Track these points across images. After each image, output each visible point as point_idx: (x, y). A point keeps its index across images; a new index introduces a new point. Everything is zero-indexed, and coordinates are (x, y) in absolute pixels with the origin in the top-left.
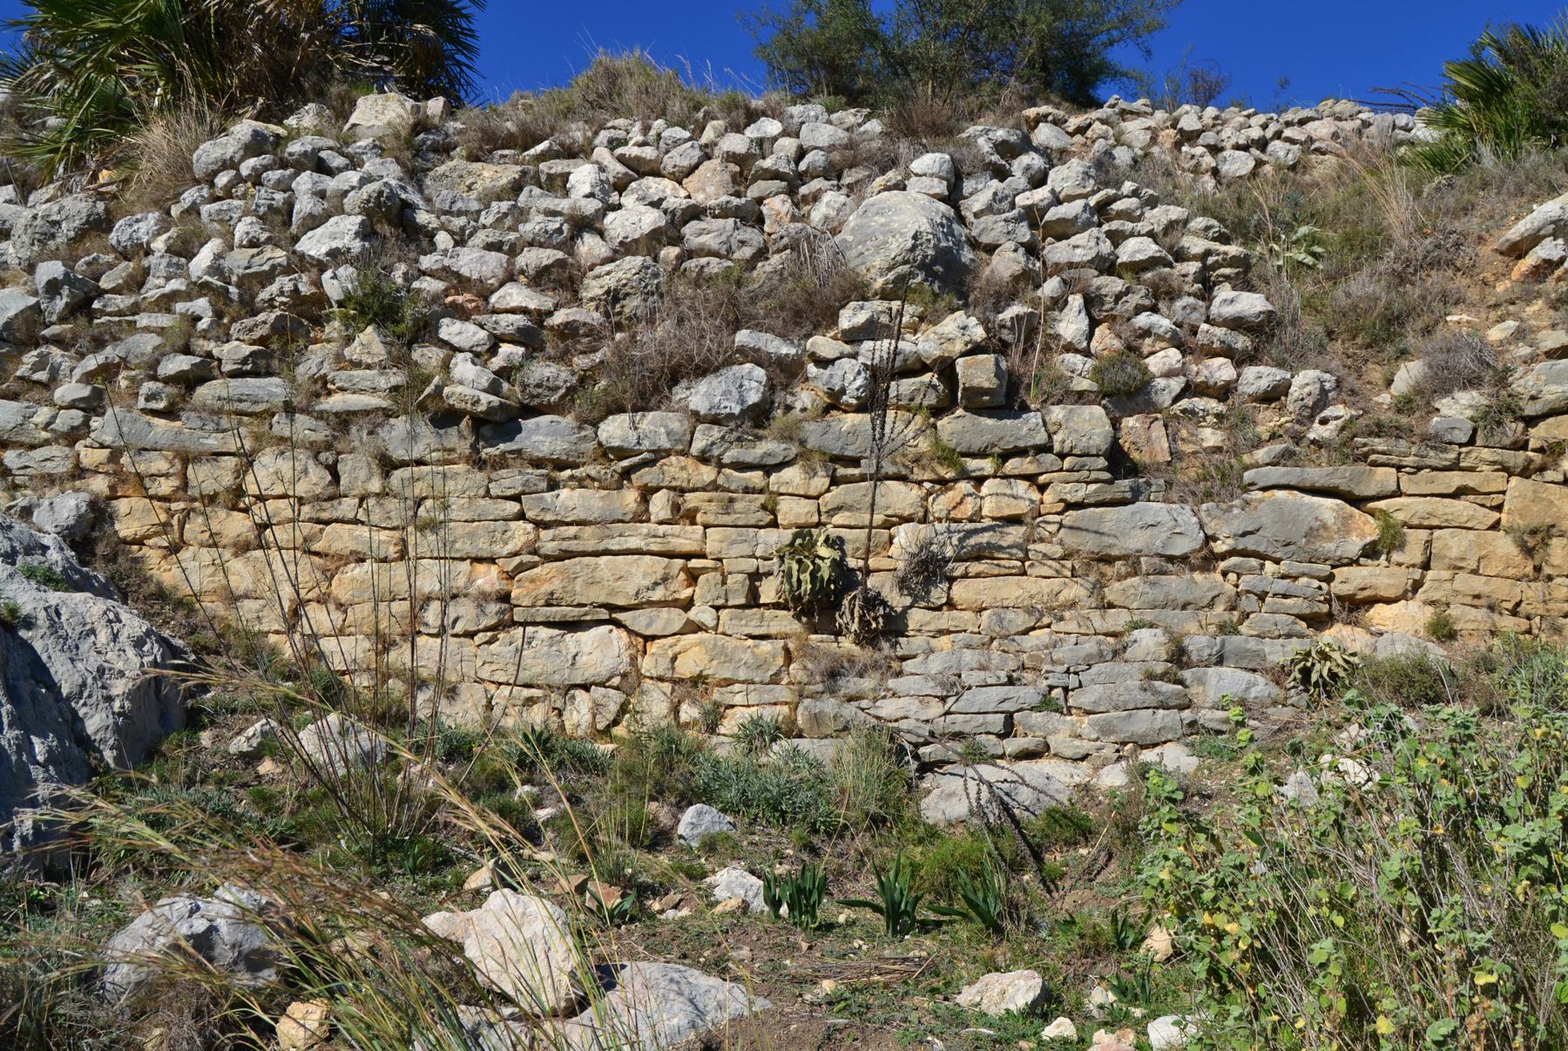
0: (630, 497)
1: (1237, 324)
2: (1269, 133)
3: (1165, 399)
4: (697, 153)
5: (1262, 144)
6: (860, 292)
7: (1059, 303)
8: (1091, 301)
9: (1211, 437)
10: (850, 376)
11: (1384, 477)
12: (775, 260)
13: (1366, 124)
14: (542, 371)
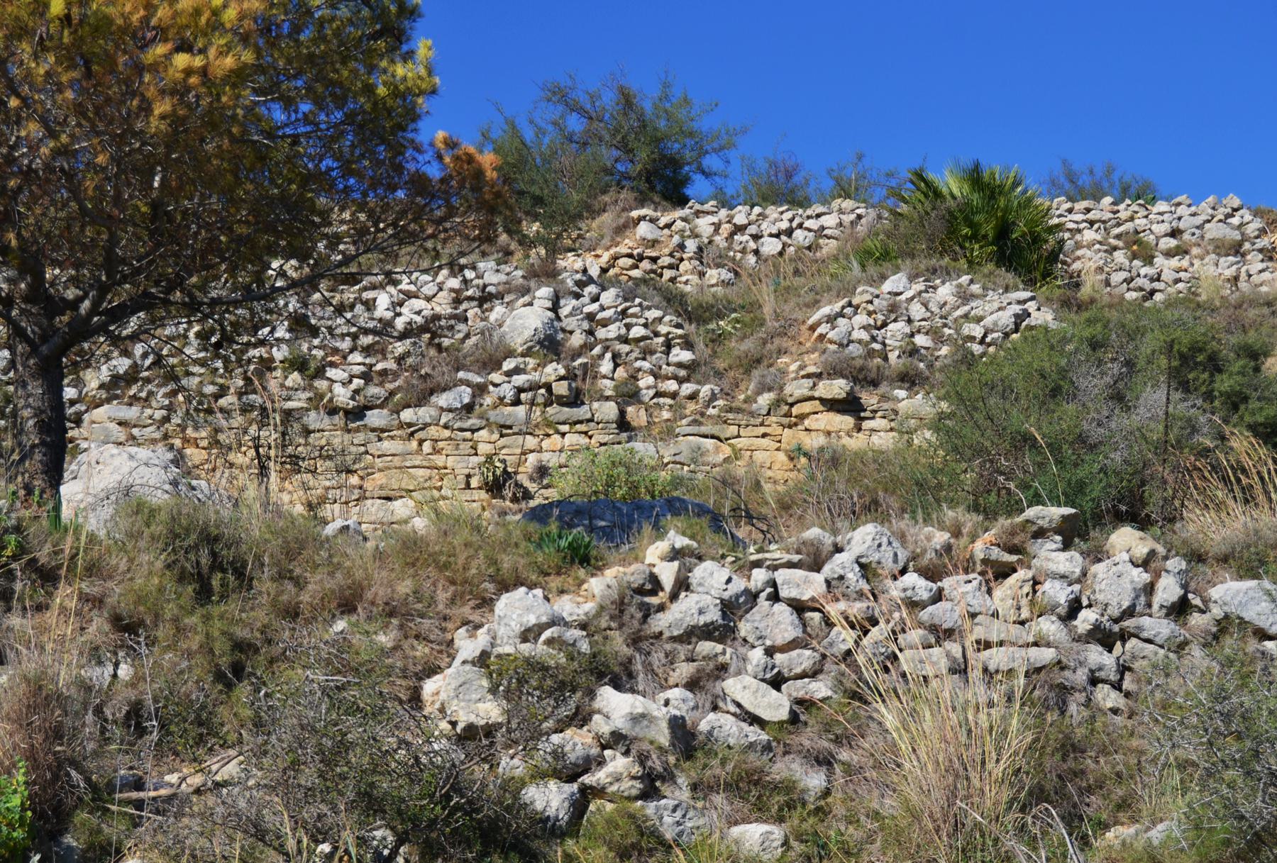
0: (414, 444)
1: (680, 365)
2: (794, 225)
3: (646, 399)
4: (436, 288)
5: (789, 232)
6: (510, 354)
7: (601, 356)
8: (615, 357)
9: (666, 415)
10: (507, 391)
11: (733, 430)
12: (473, 340)
13: (859, 217)
14: (373, 390)
